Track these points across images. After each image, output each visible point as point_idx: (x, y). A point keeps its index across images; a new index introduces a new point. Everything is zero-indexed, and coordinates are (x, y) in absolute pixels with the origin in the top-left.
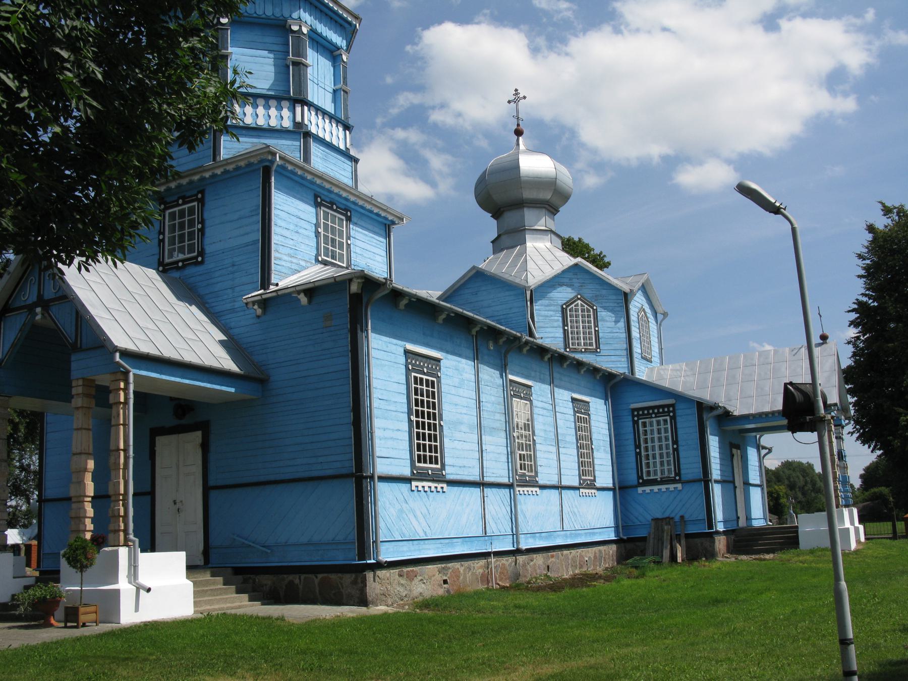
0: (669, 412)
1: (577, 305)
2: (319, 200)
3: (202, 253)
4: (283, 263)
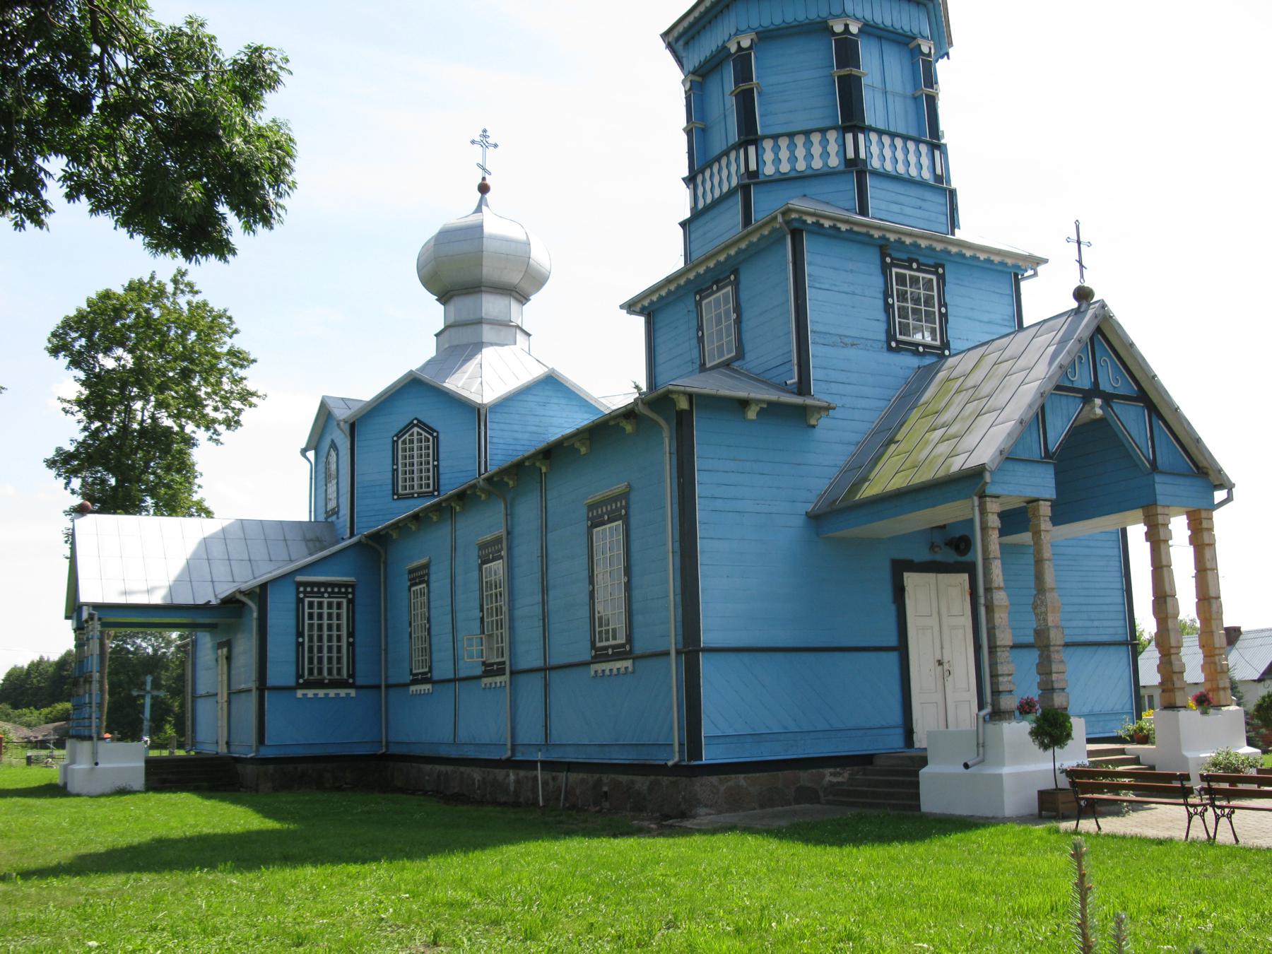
0: (347, 593)
1: (412, 435)
2: (888, 260)
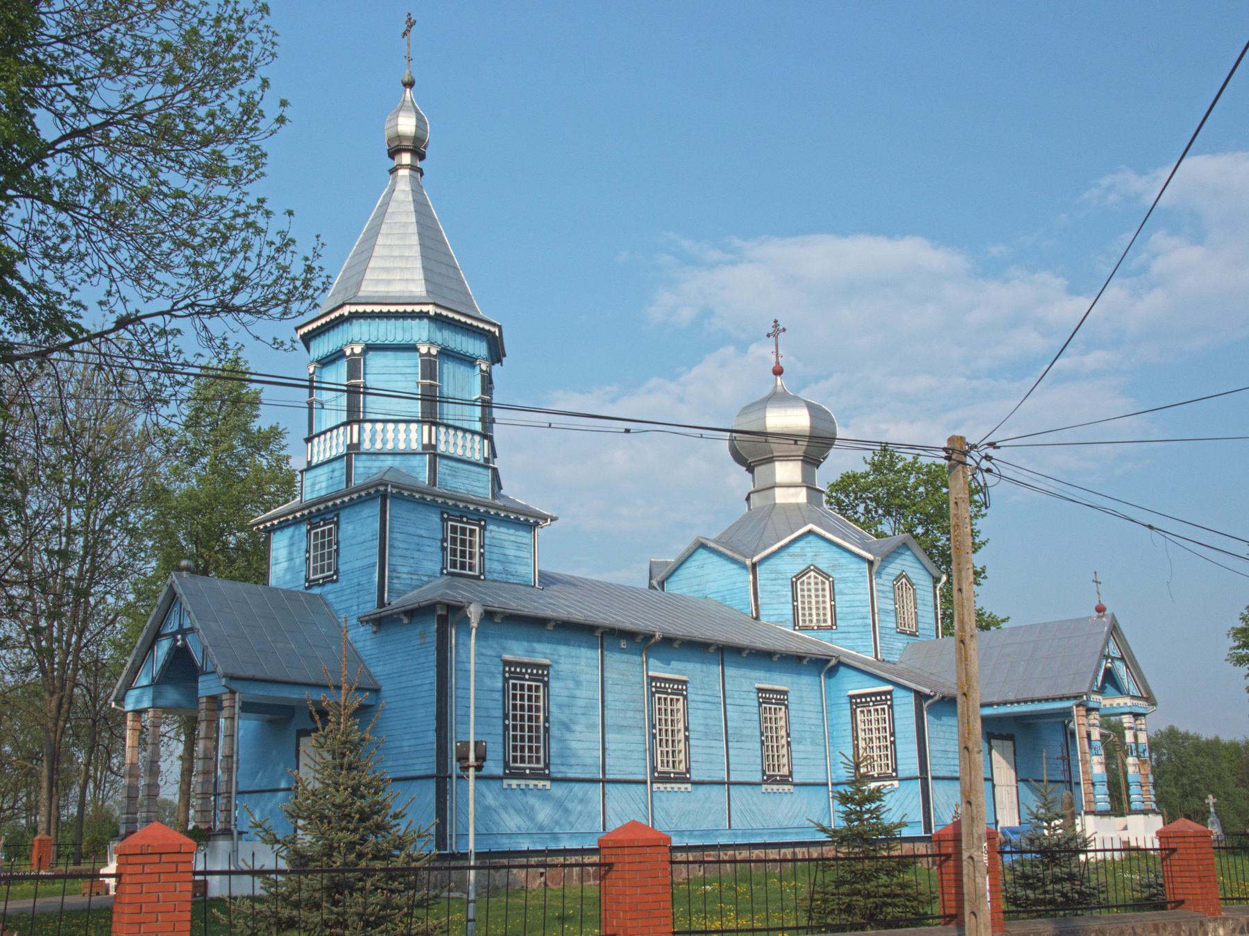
3: (336, 572)
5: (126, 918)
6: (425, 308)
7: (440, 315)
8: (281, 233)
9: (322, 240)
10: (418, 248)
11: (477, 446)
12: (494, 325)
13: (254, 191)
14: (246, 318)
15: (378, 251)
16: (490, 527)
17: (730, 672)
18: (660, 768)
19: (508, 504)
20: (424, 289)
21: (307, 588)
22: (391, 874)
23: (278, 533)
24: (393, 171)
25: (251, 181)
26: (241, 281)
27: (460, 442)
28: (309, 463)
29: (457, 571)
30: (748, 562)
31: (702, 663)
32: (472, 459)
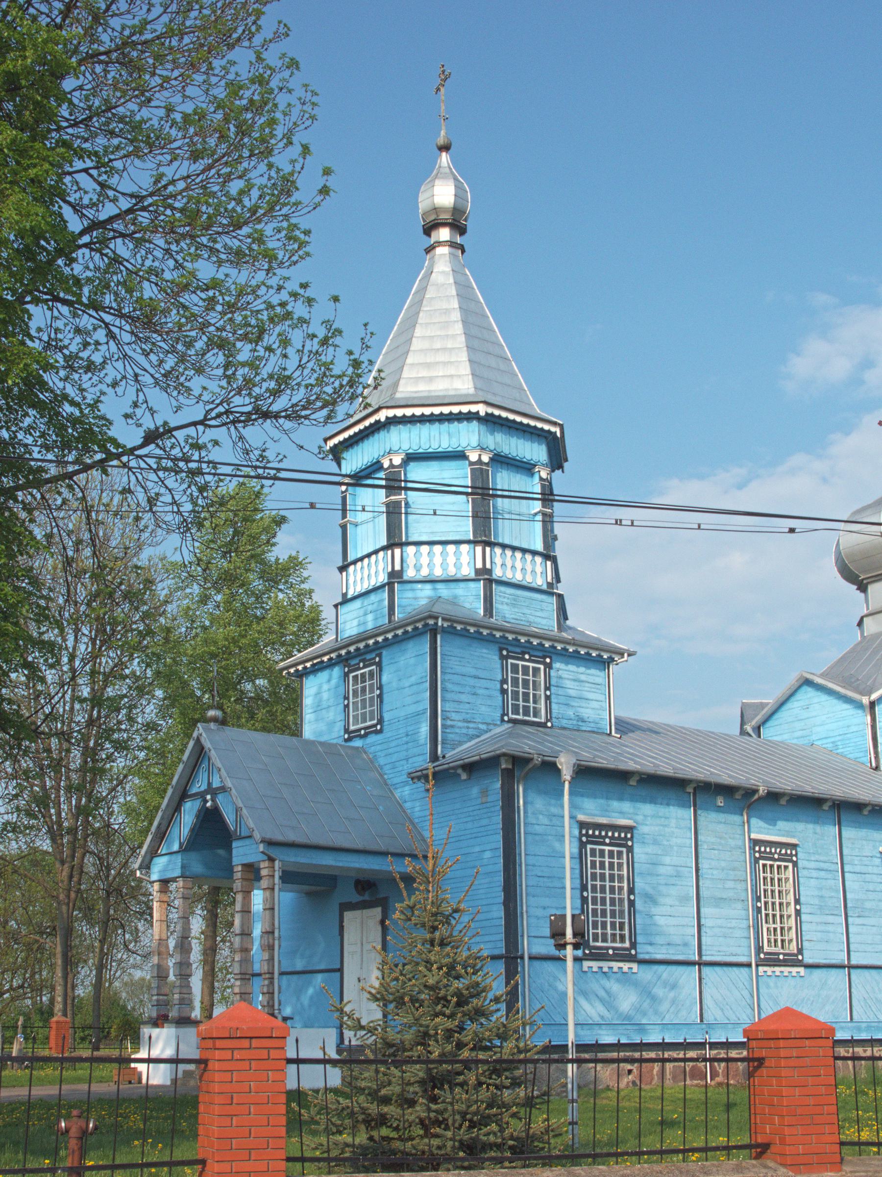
2: (505, 653)
3: (381, 721)
4: (457, 731)
5: (217, 1109)
6: (474, 408)
7: (492, 415)
8: (327, 323)
9: (370, 328)
10: (463, 338)
11: (539, 569)
12: (555, 424)
13: (296, 275)
14: (288, 425)
15: (416, 345)
16: (557, 665)
17: (848, 833)
18: (766, 948)
19: (577, 637)
20: (471, 385)
21: (346, 740)
22: (498, 1067)
23: (311, 677)
24: (430, 249)
25: (295, 263)
26: (283, 381)
27: (519, 565)
28: (344, 595)
29: (520, 717)
30: (865, 700)
31: (816, 822)
32: (534, 585)
